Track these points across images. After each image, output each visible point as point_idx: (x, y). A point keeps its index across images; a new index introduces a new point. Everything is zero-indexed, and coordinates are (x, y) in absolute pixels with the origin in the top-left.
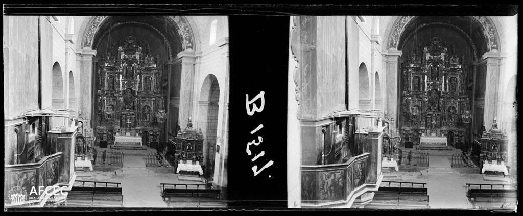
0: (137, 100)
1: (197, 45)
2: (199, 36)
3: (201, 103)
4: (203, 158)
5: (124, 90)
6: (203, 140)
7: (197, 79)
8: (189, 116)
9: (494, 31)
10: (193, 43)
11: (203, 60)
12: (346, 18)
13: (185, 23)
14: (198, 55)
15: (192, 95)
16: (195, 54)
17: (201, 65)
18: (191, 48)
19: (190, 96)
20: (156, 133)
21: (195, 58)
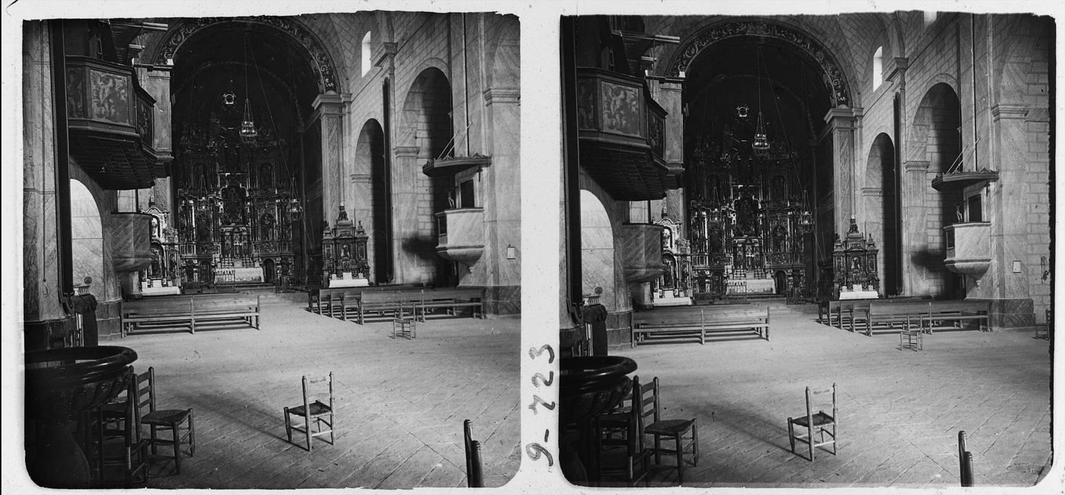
0: (250, 206)
1: (855, 98)
2: (856, 82)
3: (865, 190)
4: (879, 280)
5: (738, 201)
6: (877, 251)
7: (347, 141)
8: (340, 202)
9: (327, 62)
10: (848, 96)
11: (354, 107)
12: (1045, 73)
13: (321, 48)
14: (347, 100)
15: (852, 182)
16: (852, 113)
17: (352, 115)
18: (846, 103)
19: (339, 169)
20: (286, 259)
21: (854, 119)
